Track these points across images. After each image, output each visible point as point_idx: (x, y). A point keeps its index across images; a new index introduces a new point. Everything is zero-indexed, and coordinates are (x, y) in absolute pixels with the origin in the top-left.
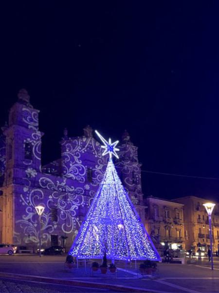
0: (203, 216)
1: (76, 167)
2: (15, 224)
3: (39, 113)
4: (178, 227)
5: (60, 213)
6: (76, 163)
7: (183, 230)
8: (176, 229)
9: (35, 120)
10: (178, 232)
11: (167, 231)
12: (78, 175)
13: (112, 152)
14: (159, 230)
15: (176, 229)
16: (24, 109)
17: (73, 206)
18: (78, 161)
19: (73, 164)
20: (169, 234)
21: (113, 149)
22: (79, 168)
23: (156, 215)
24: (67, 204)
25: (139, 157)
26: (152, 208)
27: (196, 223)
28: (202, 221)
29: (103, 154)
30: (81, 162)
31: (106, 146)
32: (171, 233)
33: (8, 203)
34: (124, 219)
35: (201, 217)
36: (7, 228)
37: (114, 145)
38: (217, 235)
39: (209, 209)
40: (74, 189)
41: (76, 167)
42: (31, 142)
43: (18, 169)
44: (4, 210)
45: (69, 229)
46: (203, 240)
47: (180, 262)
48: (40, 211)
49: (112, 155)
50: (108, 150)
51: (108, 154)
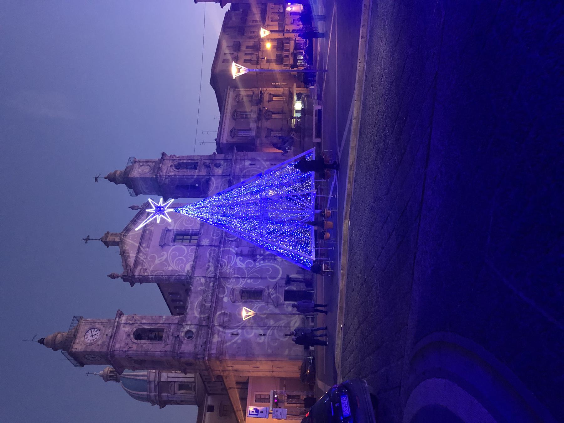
0: (246, 54)
1: (173, 262)
4: (266, 97)
5: (250, 283)
6: (166, 260)
7: (271, 89)
8: (269, 101)
10: (274, 98)
11: (274, 116)
13: (166, 209)
14: (272, 131)
15: (269, 101)
17: (238, 264)
18: (164, 258)
19: (169, 265)
20: (278, 113)
21: (160, 207)
22: (174, 257)
23: (246, 134)
24: (234, 274)
26: (235, 140)
27: (259, 66)
28: (254, 58)
29: (170, 220)
30: (165, 253)
31: (157, 215)
32: (270, 26)
33: (236, 367)
34: (260, 195)
35: (248, 57)
36: (275, 369)
37: (155, 205)
38: (280, 132)
39: (241, 70)
40: (210, 264)
41: (173, 262)
44: (247, 374)
45: (277, 271)
46: (287, 56)
47: (319, 111)
48: (249, 314)
49: (169, 208)
50: (164, 214)
51: (168, 213)
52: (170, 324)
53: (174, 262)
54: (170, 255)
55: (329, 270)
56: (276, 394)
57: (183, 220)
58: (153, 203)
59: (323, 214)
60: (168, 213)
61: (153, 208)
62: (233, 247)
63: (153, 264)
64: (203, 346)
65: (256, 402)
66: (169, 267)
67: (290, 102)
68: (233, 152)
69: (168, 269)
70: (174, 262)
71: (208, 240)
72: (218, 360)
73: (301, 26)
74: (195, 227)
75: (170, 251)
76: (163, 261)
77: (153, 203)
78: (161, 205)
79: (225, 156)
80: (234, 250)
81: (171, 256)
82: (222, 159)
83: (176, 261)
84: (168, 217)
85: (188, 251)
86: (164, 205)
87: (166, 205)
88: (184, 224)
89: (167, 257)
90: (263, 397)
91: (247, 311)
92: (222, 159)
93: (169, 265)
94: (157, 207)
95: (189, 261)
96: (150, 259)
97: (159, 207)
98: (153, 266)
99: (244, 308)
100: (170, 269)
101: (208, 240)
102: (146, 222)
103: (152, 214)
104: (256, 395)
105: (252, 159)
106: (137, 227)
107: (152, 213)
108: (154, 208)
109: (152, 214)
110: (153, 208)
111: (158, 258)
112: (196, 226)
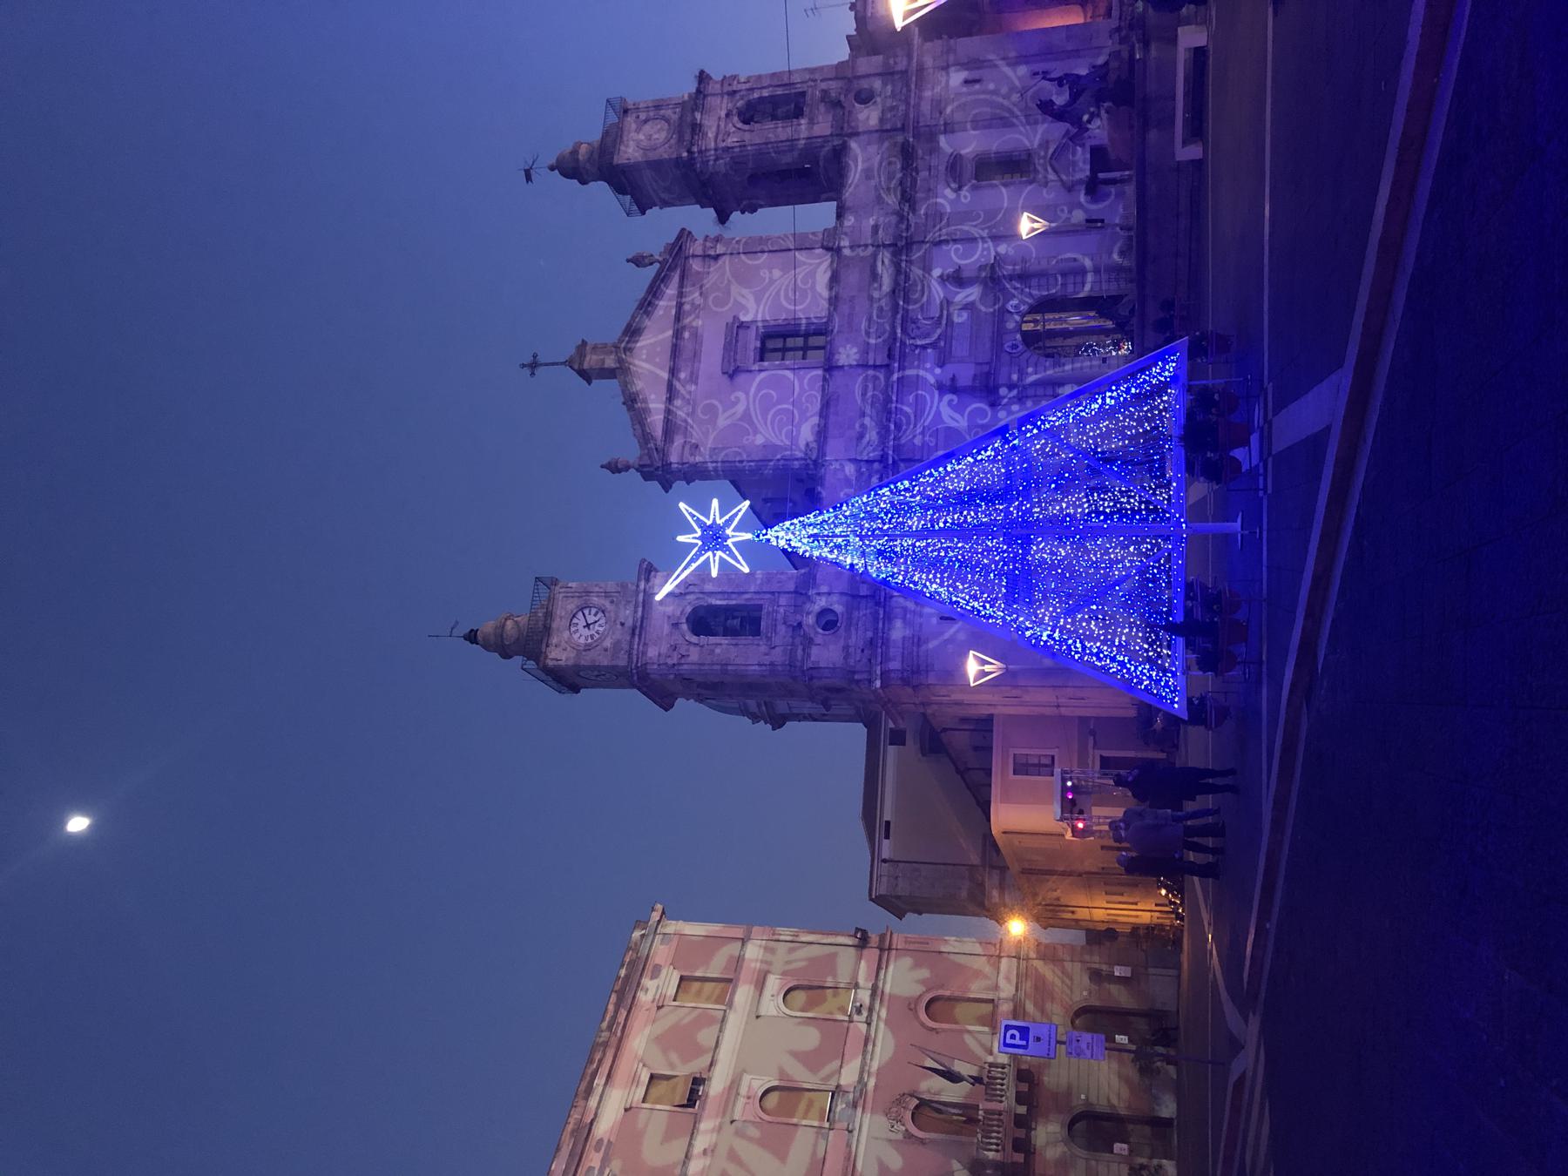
6: (746, 416)
18: (740, 408)
19: (756, 431)
36: (1062, 701)
44: (985, 711)
52: (776, 594)
56: (1071, 779)
58: (693, 516)
61: (696, 532)
65: (1014, 774)
66: (755, 435)
70: (769, 417)
75: (753, 390)
77: (693, 516)
81: (757, 402)
84: (740, 558)
93: (756, 431)
98: (715, 433)
99: (971, 652)
100: (759, 440)
101: (855, 350)
104: (1015, 755)
110: (696, 532)
111: (724, 411)
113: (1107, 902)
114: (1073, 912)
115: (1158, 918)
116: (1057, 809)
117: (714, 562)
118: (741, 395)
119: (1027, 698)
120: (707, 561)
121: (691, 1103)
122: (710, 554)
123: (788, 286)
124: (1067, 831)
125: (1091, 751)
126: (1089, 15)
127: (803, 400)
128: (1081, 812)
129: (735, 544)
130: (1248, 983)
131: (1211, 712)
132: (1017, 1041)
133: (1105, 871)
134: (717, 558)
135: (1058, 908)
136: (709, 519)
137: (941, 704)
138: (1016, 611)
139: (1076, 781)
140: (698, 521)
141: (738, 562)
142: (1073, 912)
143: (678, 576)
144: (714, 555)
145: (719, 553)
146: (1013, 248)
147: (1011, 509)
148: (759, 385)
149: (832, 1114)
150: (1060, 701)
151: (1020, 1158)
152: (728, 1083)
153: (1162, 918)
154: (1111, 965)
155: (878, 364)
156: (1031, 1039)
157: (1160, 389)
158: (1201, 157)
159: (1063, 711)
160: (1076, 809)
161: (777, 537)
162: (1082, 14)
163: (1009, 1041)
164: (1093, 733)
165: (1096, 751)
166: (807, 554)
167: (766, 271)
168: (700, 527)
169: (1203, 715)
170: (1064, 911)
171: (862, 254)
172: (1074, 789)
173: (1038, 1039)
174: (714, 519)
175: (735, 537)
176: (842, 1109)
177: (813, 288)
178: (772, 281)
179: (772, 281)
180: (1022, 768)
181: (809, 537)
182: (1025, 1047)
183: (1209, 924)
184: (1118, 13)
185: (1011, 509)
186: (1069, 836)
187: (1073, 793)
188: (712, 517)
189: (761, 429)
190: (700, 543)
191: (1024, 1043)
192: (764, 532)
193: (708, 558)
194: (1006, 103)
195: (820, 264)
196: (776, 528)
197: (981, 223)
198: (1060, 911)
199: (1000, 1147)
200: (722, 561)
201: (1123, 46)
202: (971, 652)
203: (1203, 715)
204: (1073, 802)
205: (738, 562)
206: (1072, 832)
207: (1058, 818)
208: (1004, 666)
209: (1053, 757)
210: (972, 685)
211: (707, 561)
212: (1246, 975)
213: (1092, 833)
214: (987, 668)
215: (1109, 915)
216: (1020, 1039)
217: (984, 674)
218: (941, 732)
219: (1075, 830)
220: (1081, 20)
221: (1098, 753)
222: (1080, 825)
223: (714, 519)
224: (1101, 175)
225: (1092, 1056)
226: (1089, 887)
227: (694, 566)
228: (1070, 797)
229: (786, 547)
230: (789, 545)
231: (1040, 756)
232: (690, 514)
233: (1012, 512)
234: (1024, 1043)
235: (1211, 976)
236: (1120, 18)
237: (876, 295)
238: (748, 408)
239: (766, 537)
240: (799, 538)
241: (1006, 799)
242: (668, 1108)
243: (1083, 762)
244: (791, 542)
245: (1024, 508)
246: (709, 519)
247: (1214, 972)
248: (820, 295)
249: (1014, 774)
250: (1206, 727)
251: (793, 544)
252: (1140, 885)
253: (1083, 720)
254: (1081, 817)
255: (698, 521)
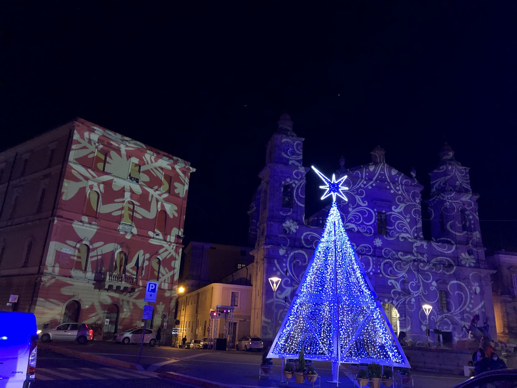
1: (356, 212)
2: (266, 305)
3: (304, 142)
6: (359, 206)
9: (298, 152)
12: (362, 224)
16: (284, 140)
18: (361, 203)
19: (353, 209)
21: (338, 188)
22: (363, 213)
25: (472, 184)
26: (505, 272)
36: (257, 310)
42: (291, 182)
43: (272, 223)
44: (254, 284)
53: (357, 213)
54: (365, 209)
55: (261, 374)
56: (230, 312)
57: (402, 220)
58: (342, 180)
59: (310, 372)
60: (331, 196)
61: (336, 181)
62: (373, 270)
63: (354, 194)
64: (276, 243)
65: (232, 292)
66: (352, 208)
67: (482, 337)
68: (490, 269)
69: (350, 207)
70: (357, 213)
71: (380, 245)
72: (264, 257)
73: (271, 361)
74: (396, 232)
76: (358, 203)
77: (342, 180)
78: (340, 188)
79: (483, 261)
80: (371, 271)
81: (365, 210)
82: (478, 257)
83: (359, 215)
84: (327, 197)
85: (369, 225)
86: (340, 191)
87: (341, 194)
88: (398, 222)
89: (362, 206)
90: (236, 299)
91: (277, 283)
92: (478, 257)
93: (353, 209)
94: (338, 184)
95: (358, 227)
96: (360, 191)
97: (338, 186)
99: (280, 280)
100: (350, 209)
101: (380, 245)
102: (321, 175)
103: (329, 180)
105: (482, 293)
106: (315, 167)
107: (331, 180)
108: (336, 182)
109: (329, 180)
110: (336, 181)
111: (361, 198)
112: (396, 233)
113: (186, 322)
114: (183, 310)
115: (180, 339)
116: (220, 305)
117: (325, 187)
118: (366, 204)
119: (258, 298)
120: (325, 185)
121: (131, 178)
122: (328, 186)
123: (404, 223)
124: (213, 309)
125: (238, 319)
126: (499, 335)
127: (363, 226)
128: (219, 315)
129: (331, 195)
130: (170, 373)
131: (267, 367)
132: (151, 288)
133: (197, 321)
134: (326, 188)
135: (185, 304)
136: (341, 186)
137: (257, 268)
138: (307, 296)
139: (230, 313)
140: (340, 182)
141: (325, 196)
142: (183, 310)
143: (321, 175)
144: (328, 187)
145: (340, 186)
146: (413, 304)
147: (346, 297)
148: (370, 211)
149: (124, 224)
150: (257, 310)
151: (107, 287)
152: (135, 192)
153: (180, 340)
154: (167, 322)
155: (376, 252)
156: (152, 293)
157: (386, 356)
158: (465, 375)
159: (253, 311)
160: (220, 313)
161: (334, 210)
162: (500, 332)
163: (151, 285)
164: (245, 320)
165: (239, 321)
166: (327, 221)
167: (409, 217)
168: (338, 183)
169: (267, 364)
170: (184, 306)
171: (414, 250)
172: (227, 312)
173: (151, 296)
174: (341, 188)
175: (334, 195)
176: (126, 228)
177: (403, 232)
178: (406, 218)
179: (406, 218)
180: (234, 295)
181: (334, 222)
182: (149, 291)
183: (186, 359)
184: (512, 346)
185: (346, 297)
186: (211, 310)
187: (226, 312)
188: (342, 187)
189: (354, 210)
190: (332, 183)
191: (150, 290)
192: (336, 206)
193: (326, 185)
194: (468, 303)
195: (411, 235)
196: (337, 210)
197: (422, 293)
198: (184, 305)
199: (110, 280)
200: (325, 190)
201: (500, 347)
202: (280, 280)
203: (267, 364)
204: (223, 312)
205: (325, 196)
206: (213, 311)
207: (218, 307)
208: (275, 291)
209: (237, 306)
210: (269, 279)
211: (325, 185)
212: (172, 373)
213: (212, 318)
214: (275, 285)
215: (182, 322)
216: (151, 289)
217: (273, 283)
218: (247, 268)
219: (213, 312)
220: (498, 331)
221: (238, 322)
222: (215, 314)
223: (341, 188)
224: (441, 336)
225: (144, 314)
226: (192, 316)
227: (324, 180)
228: (225, 311)
229: (330, 213)
230: (331, 215)
231: (238, 301)
232: (343, 180)
233: (345, 297)
234: (150, 290)
235: (169, 359)
236: (510, 347)
237: (400, 253)
238: (361, 206)
239: (334, 206)
240: (334, 218)
241: (224, 289)
242: (130, 171)
243: (236, 316)
244: (332, 215)
245: (346, 302)
246: (341, 186)
247: (170, 360)
248: (400, 234)
249: (232, 292)
250: (262, 364)
251: (332, 216)
252: (192, 333)
253: (249, 317)
254: (218, 315)
255: (340, 182)
